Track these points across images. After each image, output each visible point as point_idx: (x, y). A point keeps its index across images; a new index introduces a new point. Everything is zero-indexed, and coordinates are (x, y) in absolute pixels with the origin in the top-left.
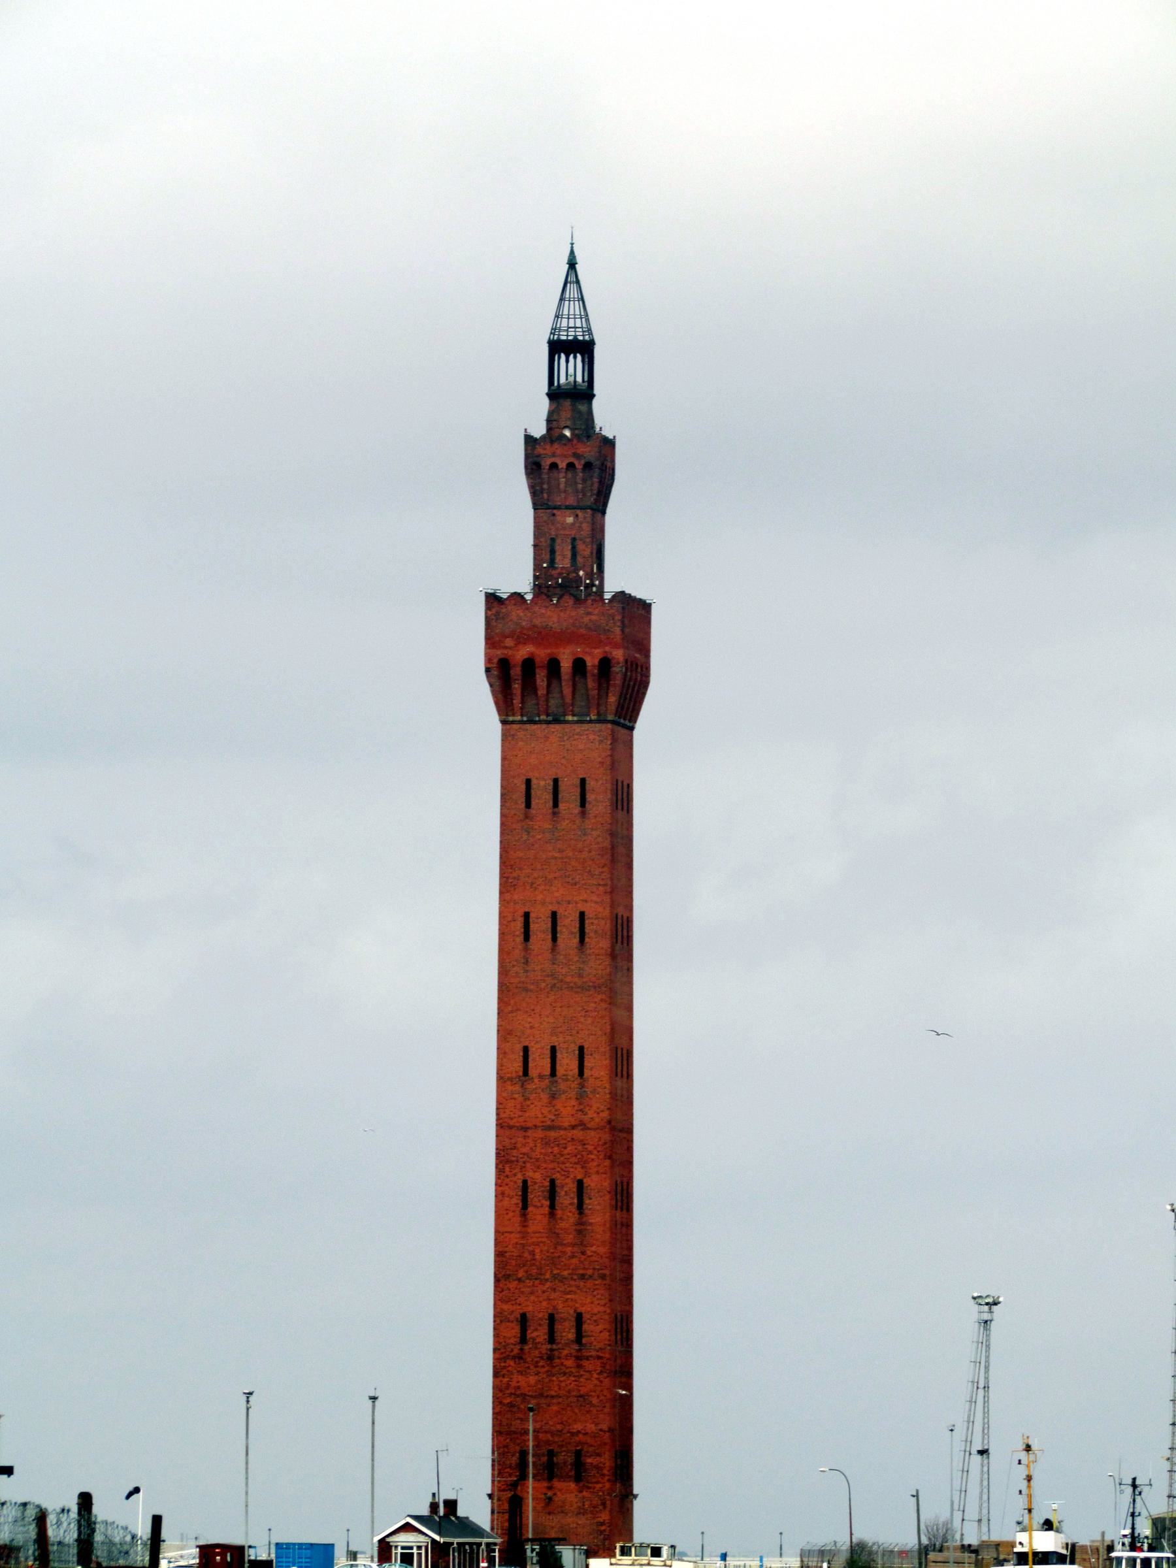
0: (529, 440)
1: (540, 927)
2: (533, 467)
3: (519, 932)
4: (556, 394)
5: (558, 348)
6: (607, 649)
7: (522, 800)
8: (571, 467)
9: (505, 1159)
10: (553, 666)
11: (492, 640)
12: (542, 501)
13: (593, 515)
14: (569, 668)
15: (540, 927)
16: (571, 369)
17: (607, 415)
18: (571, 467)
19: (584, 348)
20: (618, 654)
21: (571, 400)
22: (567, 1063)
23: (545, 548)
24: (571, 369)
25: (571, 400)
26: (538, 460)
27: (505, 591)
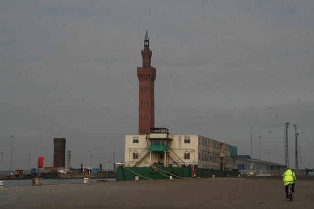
0: (142, 51)
1: (143, 103)
2: (142, 54)
3: (141, 103)
4: (145, 46)
5: (145, 41)
6: (183, 159)
7: (142, 89)
8: (147, 54)
9: (140, 127)
10: (144, 75)
11: (138, 72)
12: (144, 58)
13: (161, 148)
14: (147, 75)
15: (143, 103)
16: (147, 44)
17: (151, 48)
18: (147, 54)
19: (148, 41)
20: (151, 74)
21: (147, 47)
22: (146, 117)
23: (144, 62)
24: (147, 44)
25: (147, 47)
26: (143, 53)
27: (139, 67)
